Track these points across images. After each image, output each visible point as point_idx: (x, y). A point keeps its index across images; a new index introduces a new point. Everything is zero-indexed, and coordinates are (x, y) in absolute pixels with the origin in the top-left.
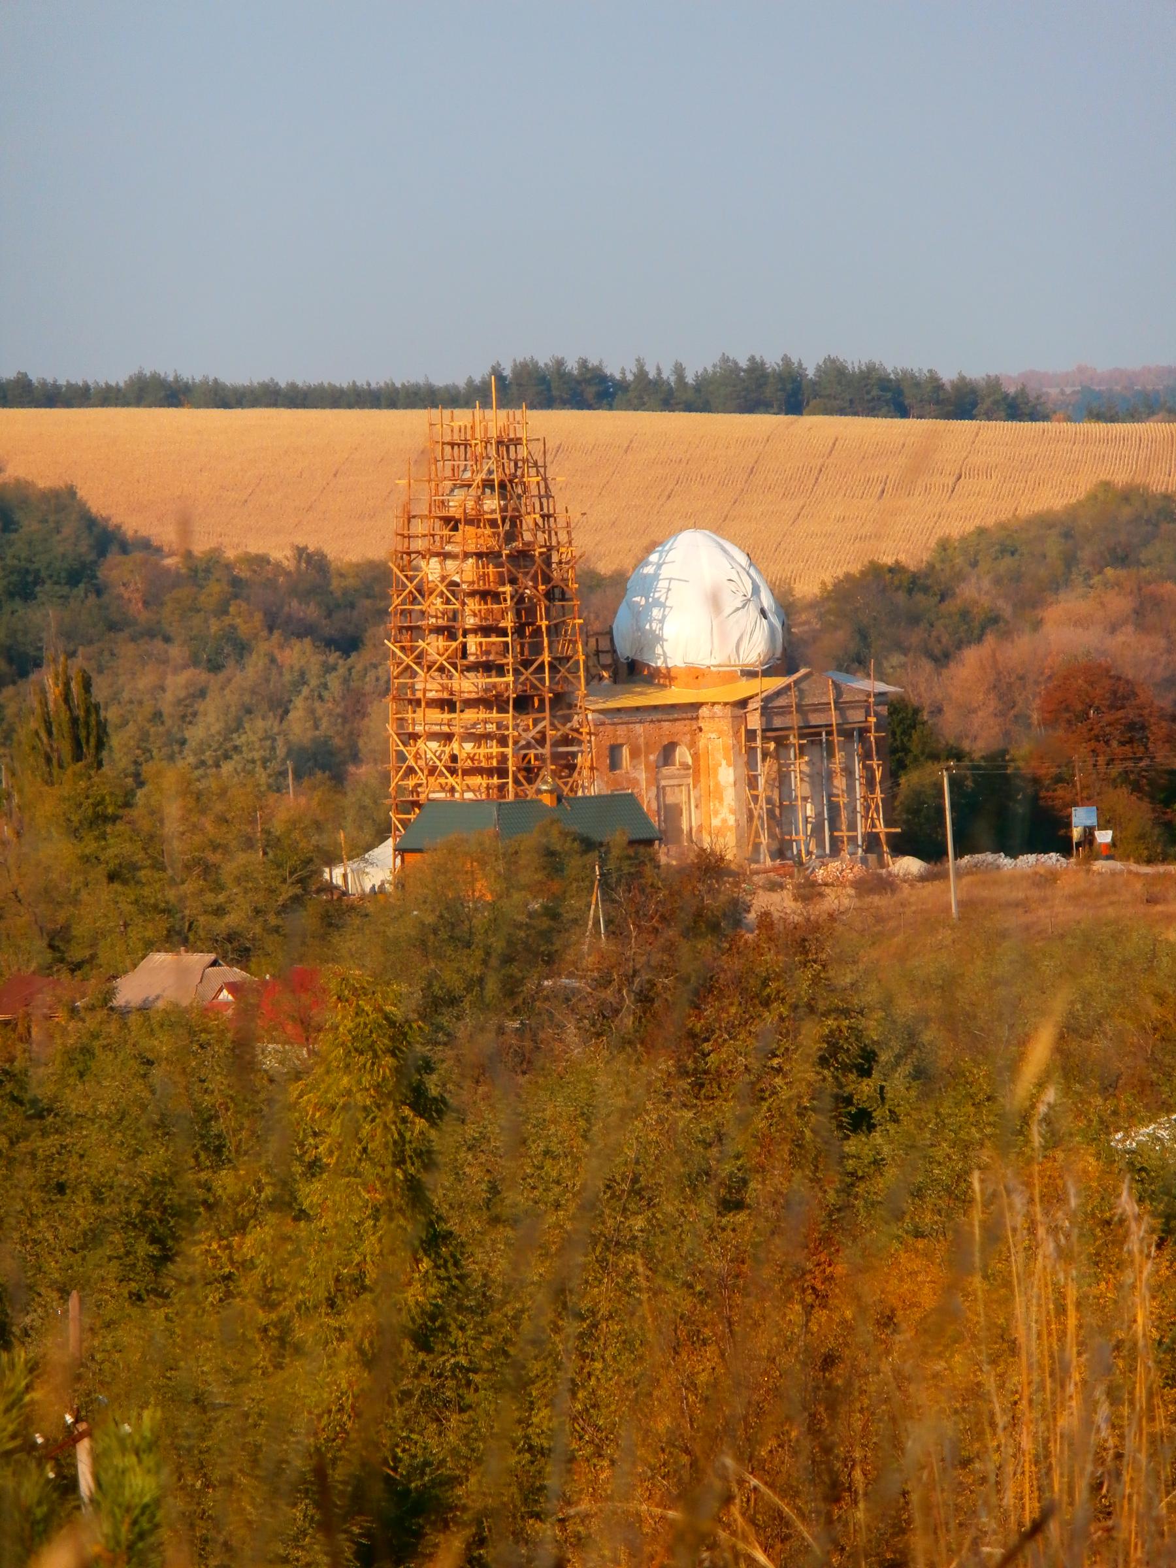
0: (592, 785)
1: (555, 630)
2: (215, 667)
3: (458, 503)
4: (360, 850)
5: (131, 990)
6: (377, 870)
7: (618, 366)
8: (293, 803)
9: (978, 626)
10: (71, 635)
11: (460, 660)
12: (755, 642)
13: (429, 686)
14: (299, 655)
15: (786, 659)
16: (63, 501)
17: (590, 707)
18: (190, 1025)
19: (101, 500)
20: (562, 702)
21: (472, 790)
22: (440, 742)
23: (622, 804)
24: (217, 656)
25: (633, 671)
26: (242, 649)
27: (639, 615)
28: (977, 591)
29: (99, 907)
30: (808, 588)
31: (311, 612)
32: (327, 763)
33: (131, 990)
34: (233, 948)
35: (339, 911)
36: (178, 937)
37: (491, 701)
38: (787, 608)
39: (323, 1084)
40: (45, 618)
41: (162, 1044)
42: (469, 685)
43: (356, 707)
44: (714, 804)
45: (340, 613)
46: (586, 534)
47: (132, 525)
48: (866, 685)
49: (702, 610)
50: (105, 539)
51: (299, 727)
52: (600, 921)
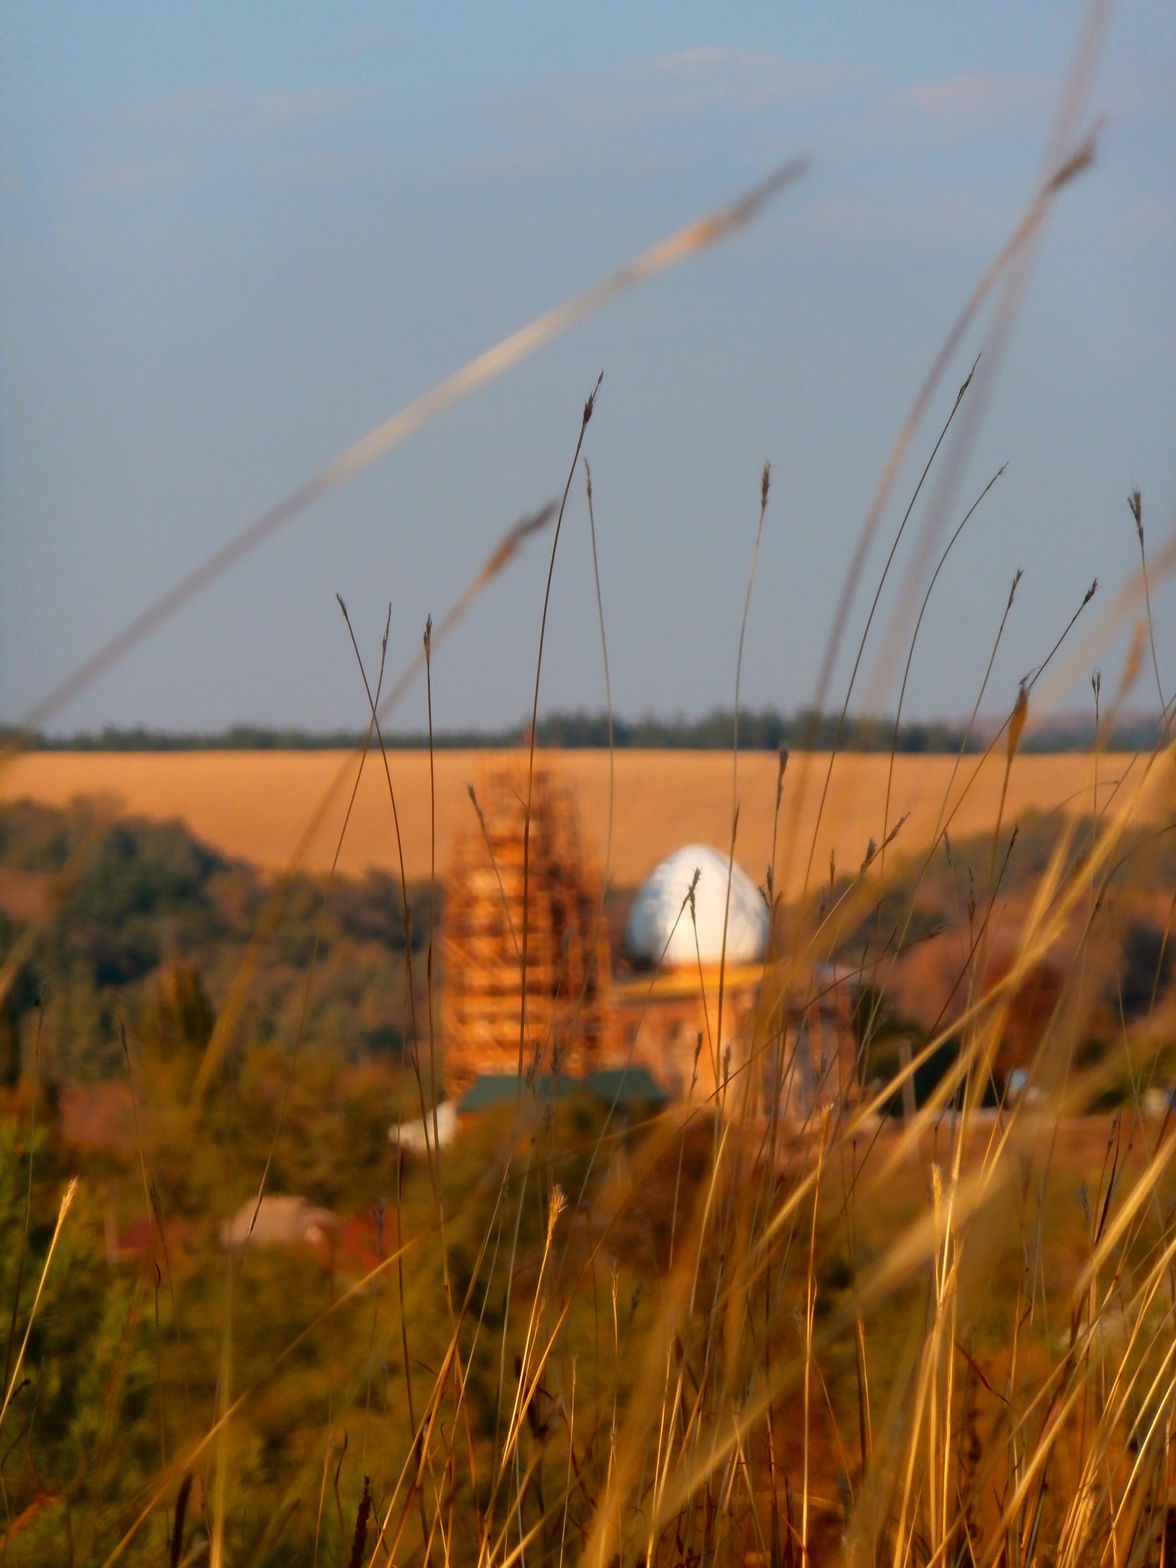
0: (613, 1058)
1: (584, 930)
2: (301, 962)
3: (501, 826)
4: (424, 1111)
5: (239, 1229)
6: (445, 1124)
7: (630, 712)
8: (365, 1076)
9: (929, 927)
10: (185, 942)
11: (503, 958)
12: (746, 940)
13: (479, 978)
14: (372, 955)
15: (772, 950)
16: (175, 831)
17: (613, 995)
18: (288, 1260)
19: (209, 829)
20: (590, 992)
21: (510, 1064)
22: (486, 1026)
23: (639, 1075)
24: (306, 955)
25: (644, 962)
26: (324, 950)
27: (651, 919)
28: (928, 896)
29: (206, 1165)
30: (793, 891)
31: (378, 919)
32: (393, 1043)
33: (239, 1229)
34: (323, 1196)
35: (406, 1164)
36: (277, 1186)
37: (527, 989)
38: (774, 906)
39: (395, 1292)
40: (165, 927)
41: (263, 1271)
42: (511, 977)
43: (418, 998)
44: (707, 1072)
45: (405, 920)
46: (605, 854)
47: (230, 846)
48: (842, 973)
49: (703, 914)
50: (209, 862)
51: (371, 1014)
52: (607, 1165)
